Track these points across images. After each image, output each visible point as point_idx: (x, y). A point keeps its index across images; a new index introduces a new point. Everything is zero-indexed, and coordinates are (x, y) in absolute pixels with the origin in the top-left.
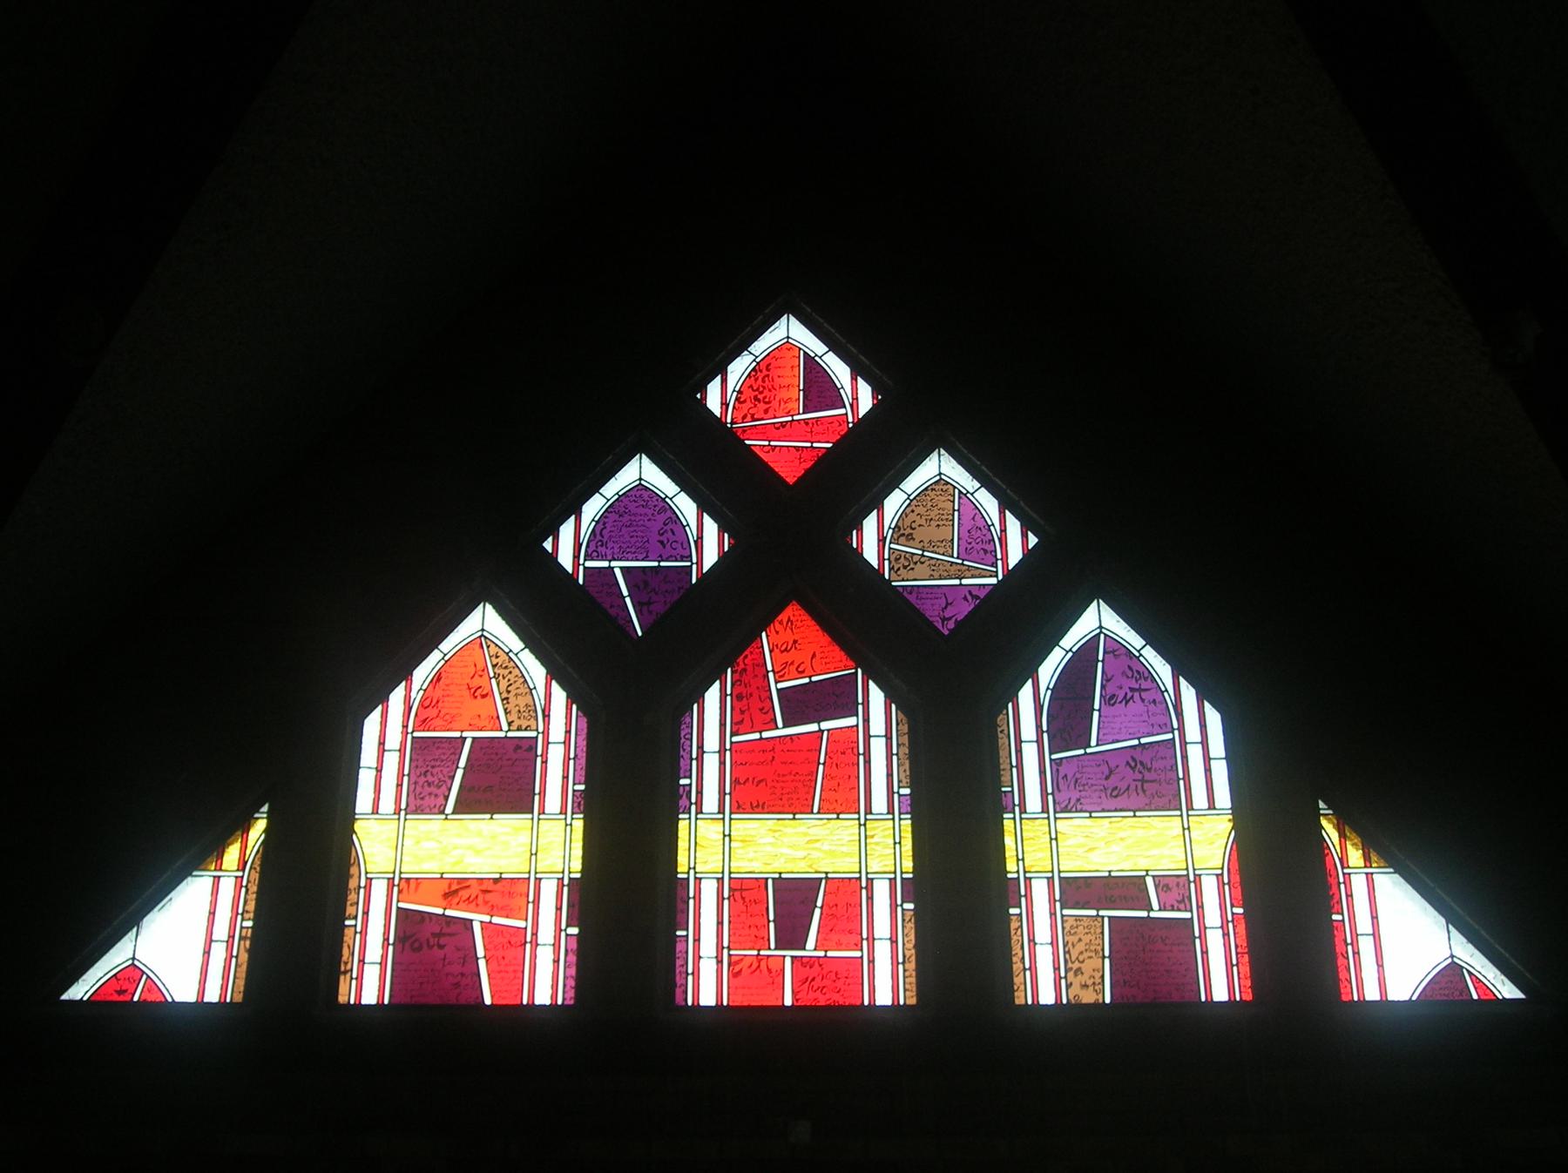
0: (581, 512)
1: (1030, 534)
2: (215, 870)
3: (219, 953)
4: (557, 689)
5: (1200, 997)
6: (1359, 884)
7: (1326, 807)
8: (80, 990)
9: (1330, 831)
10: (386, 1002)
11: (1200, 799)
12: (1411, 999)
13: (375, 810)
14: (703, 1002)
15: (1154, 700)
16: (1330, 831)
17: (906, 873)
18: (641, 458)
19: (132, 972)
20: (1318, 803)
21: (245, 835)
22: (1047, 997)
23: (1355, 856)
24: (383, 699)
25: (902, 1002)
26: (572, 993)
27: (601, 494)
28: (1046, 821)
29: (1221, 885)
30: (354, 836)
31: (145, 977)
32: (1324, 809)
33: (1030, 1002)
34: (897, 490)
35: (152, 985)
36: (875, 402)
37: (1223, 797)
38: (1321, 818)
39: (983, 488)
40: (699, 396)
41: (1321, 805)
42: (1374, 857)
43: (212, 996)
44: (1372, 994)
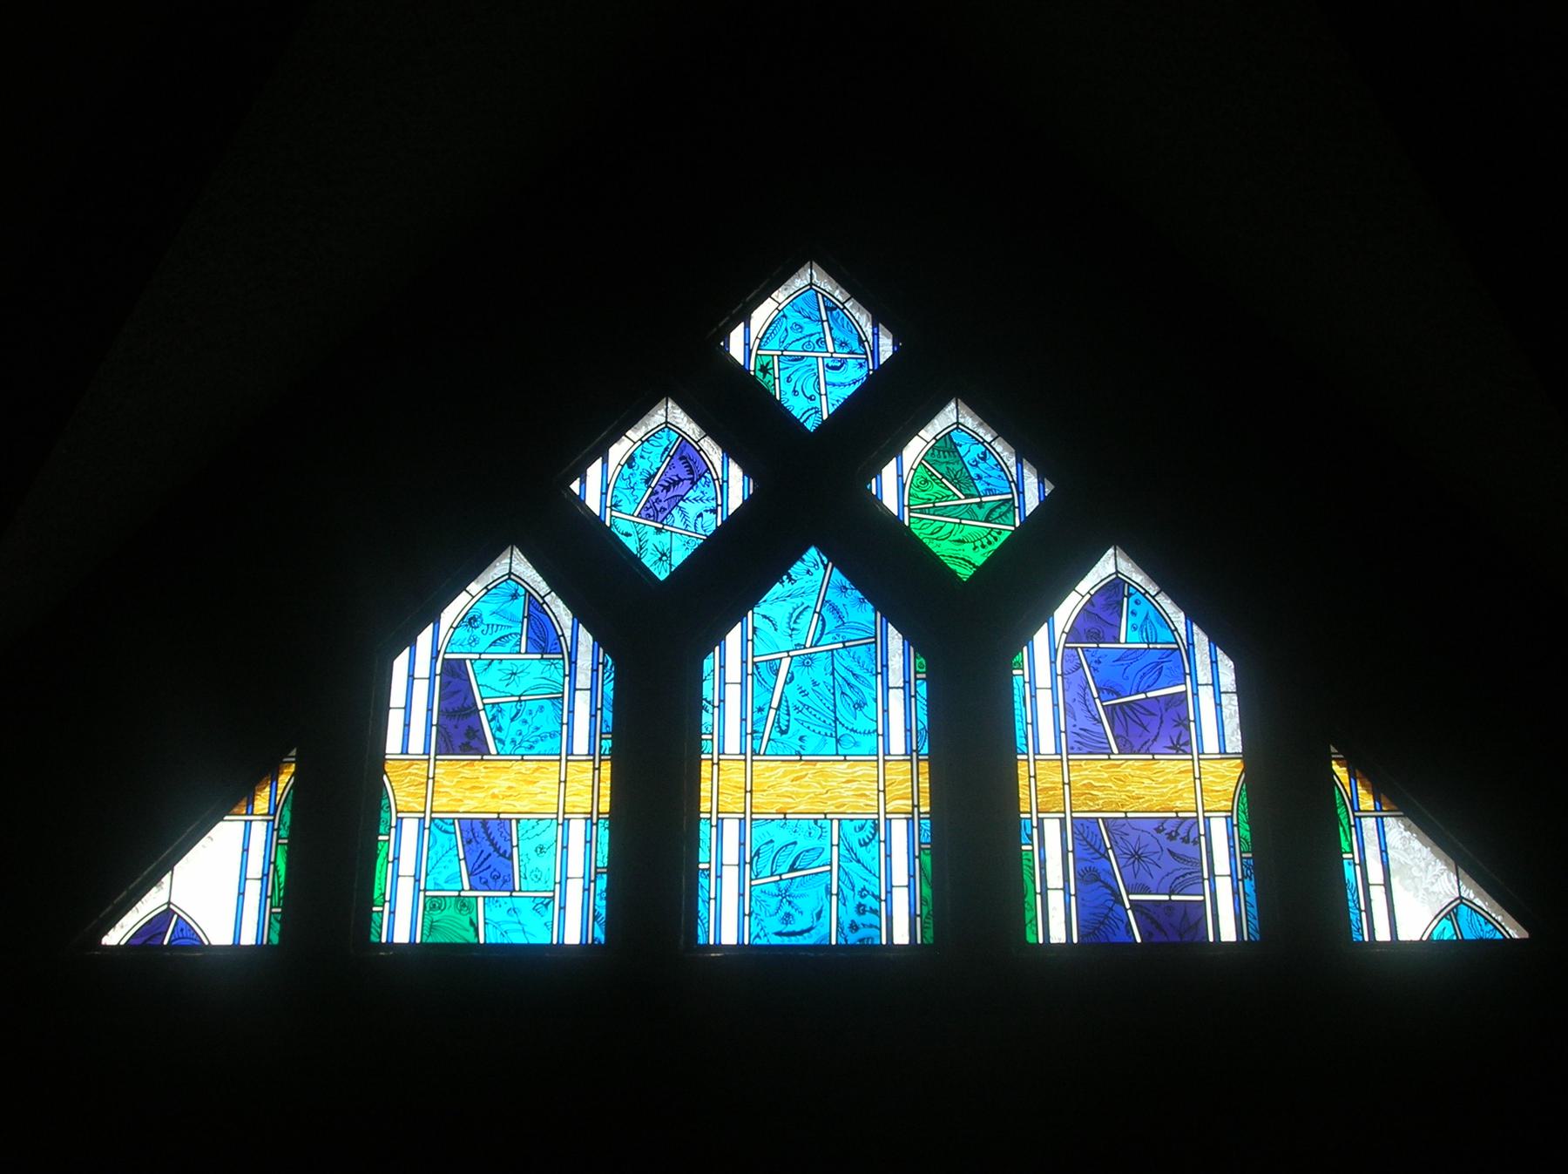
0: (586, 475)
1: (1047, 482)
2: (247, 814)
3: (253, 890)
4: (583, 632)
5: (1208, 938)
6: (1369, 824)
7: (1336, 751)
8: (114, 937)
9: (1340, 772)
10: (1075, 941)
11: (1211, 745)
12: (1421, 939)
13: (405, 751)
14: (397, 940)
15: (1100, 662)
16: (1340, 772)
17: (602, 813)
18: (512, 554)
19: (167, 913)
20: (1329, 748)
21: (274, 784)
22: (729, 937)
23: (1367, 802)
24: (412, 642)
25: (746, 942)
26: (930, 933)
27: (468, 592)
28: (1059, 763)
29: (1231, 827)
30: (385, 778)
31: (1079, 650)
32: (1335, 754)
33: (1041, 941)
34: (916, 437)
35: (185, 928)
36: (896, 349)
37: (1235, 743)
38: (1333, 762)
39: (1000, 438)
40: (722, 344)
41: (1333, 749)
42: (1384, 799)
43: (248, 938)
44: (1383, 935)
